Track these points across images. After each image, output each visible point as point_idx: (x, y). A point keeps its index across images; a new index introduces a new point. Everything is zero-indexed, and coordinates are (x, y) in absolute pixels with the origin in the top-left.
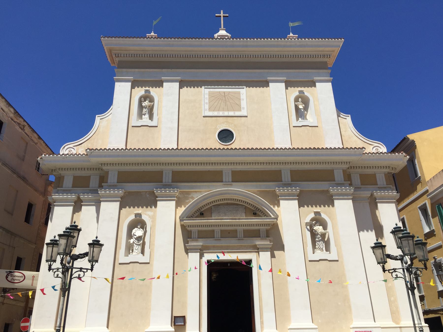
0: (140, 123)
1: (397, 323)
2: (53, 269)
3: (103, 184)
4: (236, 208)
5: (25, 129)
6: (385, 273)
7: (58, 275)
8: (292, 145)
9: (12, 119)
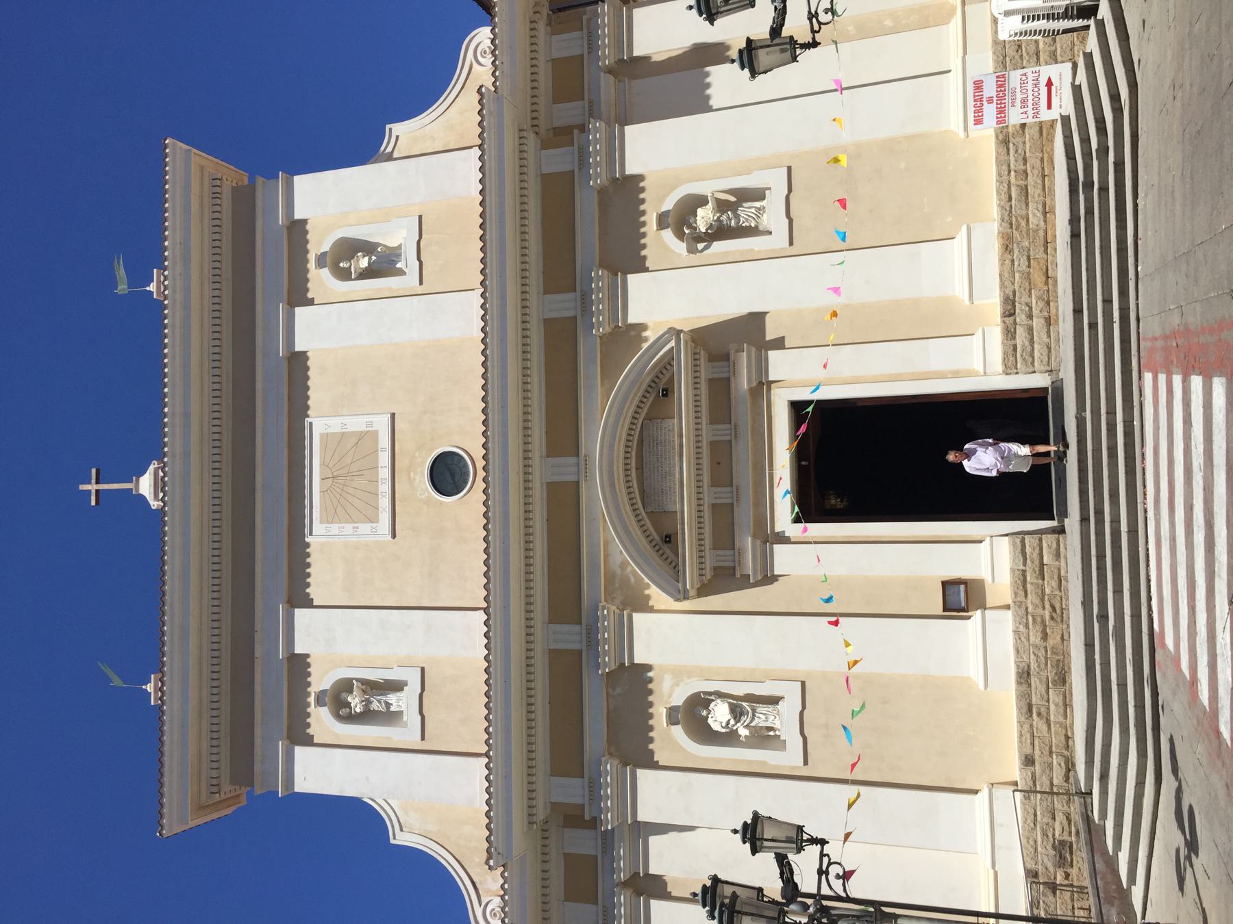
3: (587, 818)
4: (650, 445)
7: (826, 11)
8: (474, 290)
9: (1224, 214)
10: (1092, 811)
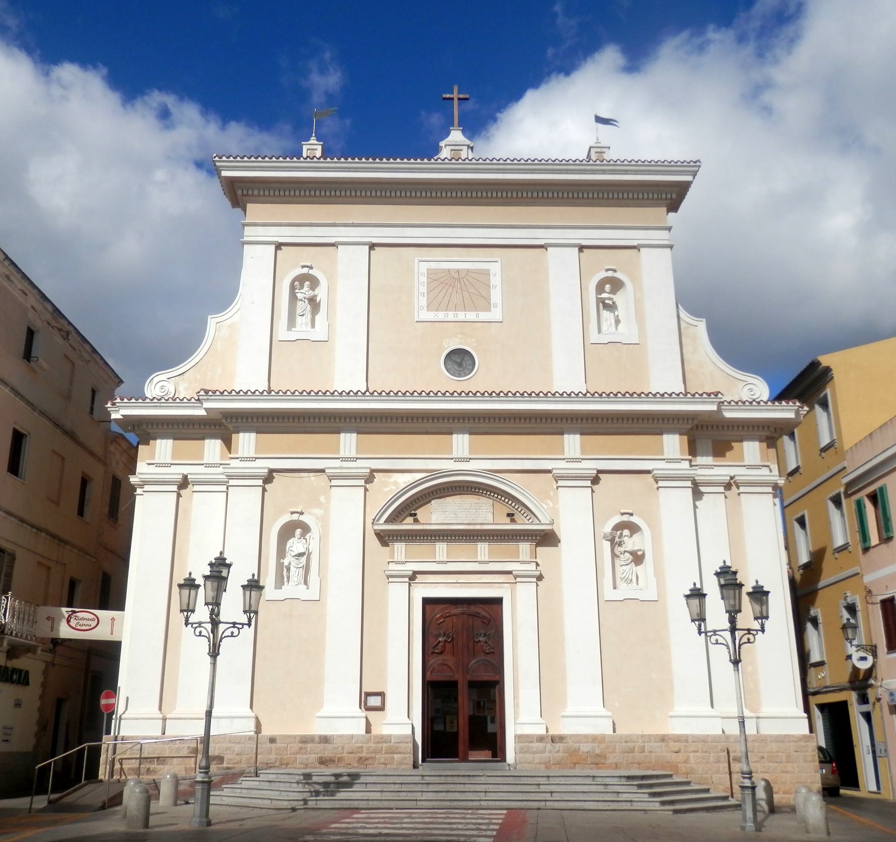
0: (292, 336)
1: (754, 712)
2: (192, 624)
4: (477, 504)
5: (69, 338)
6: (700, 635)
7: (200, 632)
8: (586, 383)
9: (49, 323)
10: (246, 777)
